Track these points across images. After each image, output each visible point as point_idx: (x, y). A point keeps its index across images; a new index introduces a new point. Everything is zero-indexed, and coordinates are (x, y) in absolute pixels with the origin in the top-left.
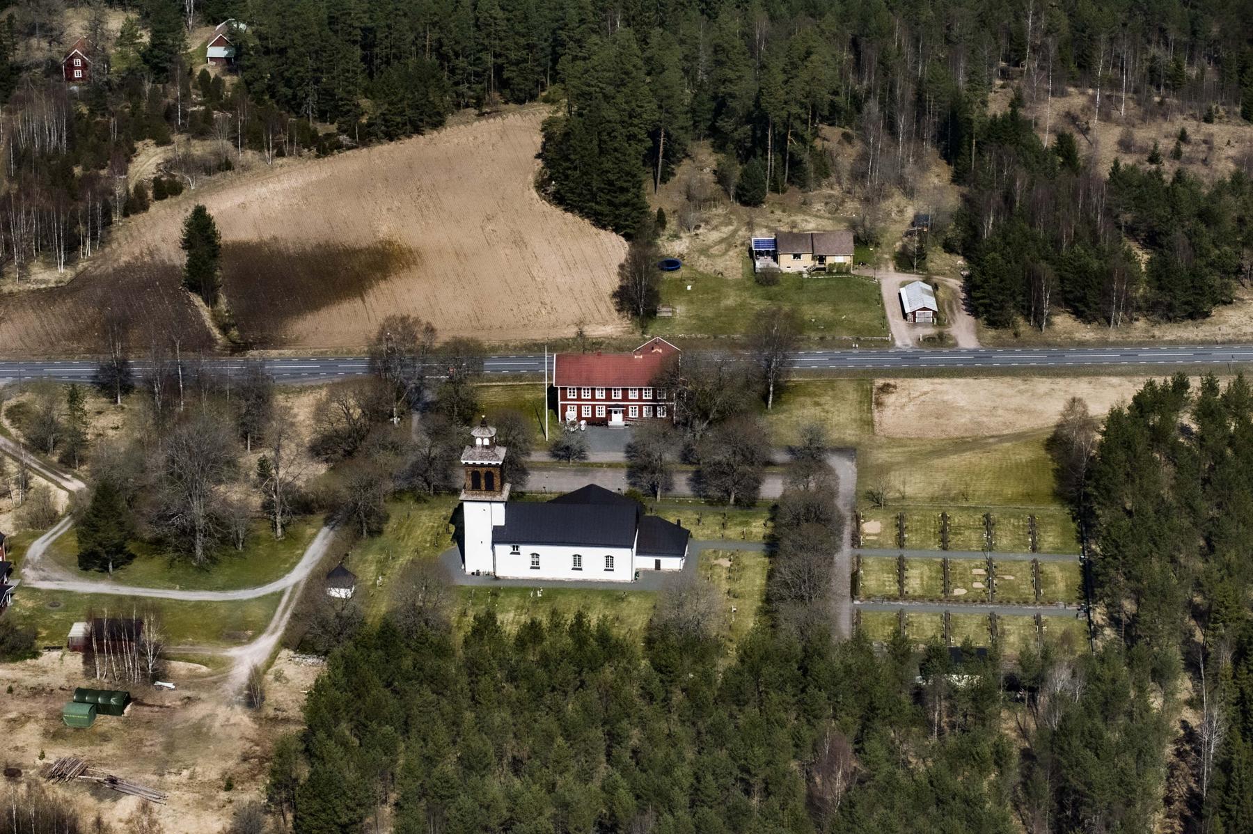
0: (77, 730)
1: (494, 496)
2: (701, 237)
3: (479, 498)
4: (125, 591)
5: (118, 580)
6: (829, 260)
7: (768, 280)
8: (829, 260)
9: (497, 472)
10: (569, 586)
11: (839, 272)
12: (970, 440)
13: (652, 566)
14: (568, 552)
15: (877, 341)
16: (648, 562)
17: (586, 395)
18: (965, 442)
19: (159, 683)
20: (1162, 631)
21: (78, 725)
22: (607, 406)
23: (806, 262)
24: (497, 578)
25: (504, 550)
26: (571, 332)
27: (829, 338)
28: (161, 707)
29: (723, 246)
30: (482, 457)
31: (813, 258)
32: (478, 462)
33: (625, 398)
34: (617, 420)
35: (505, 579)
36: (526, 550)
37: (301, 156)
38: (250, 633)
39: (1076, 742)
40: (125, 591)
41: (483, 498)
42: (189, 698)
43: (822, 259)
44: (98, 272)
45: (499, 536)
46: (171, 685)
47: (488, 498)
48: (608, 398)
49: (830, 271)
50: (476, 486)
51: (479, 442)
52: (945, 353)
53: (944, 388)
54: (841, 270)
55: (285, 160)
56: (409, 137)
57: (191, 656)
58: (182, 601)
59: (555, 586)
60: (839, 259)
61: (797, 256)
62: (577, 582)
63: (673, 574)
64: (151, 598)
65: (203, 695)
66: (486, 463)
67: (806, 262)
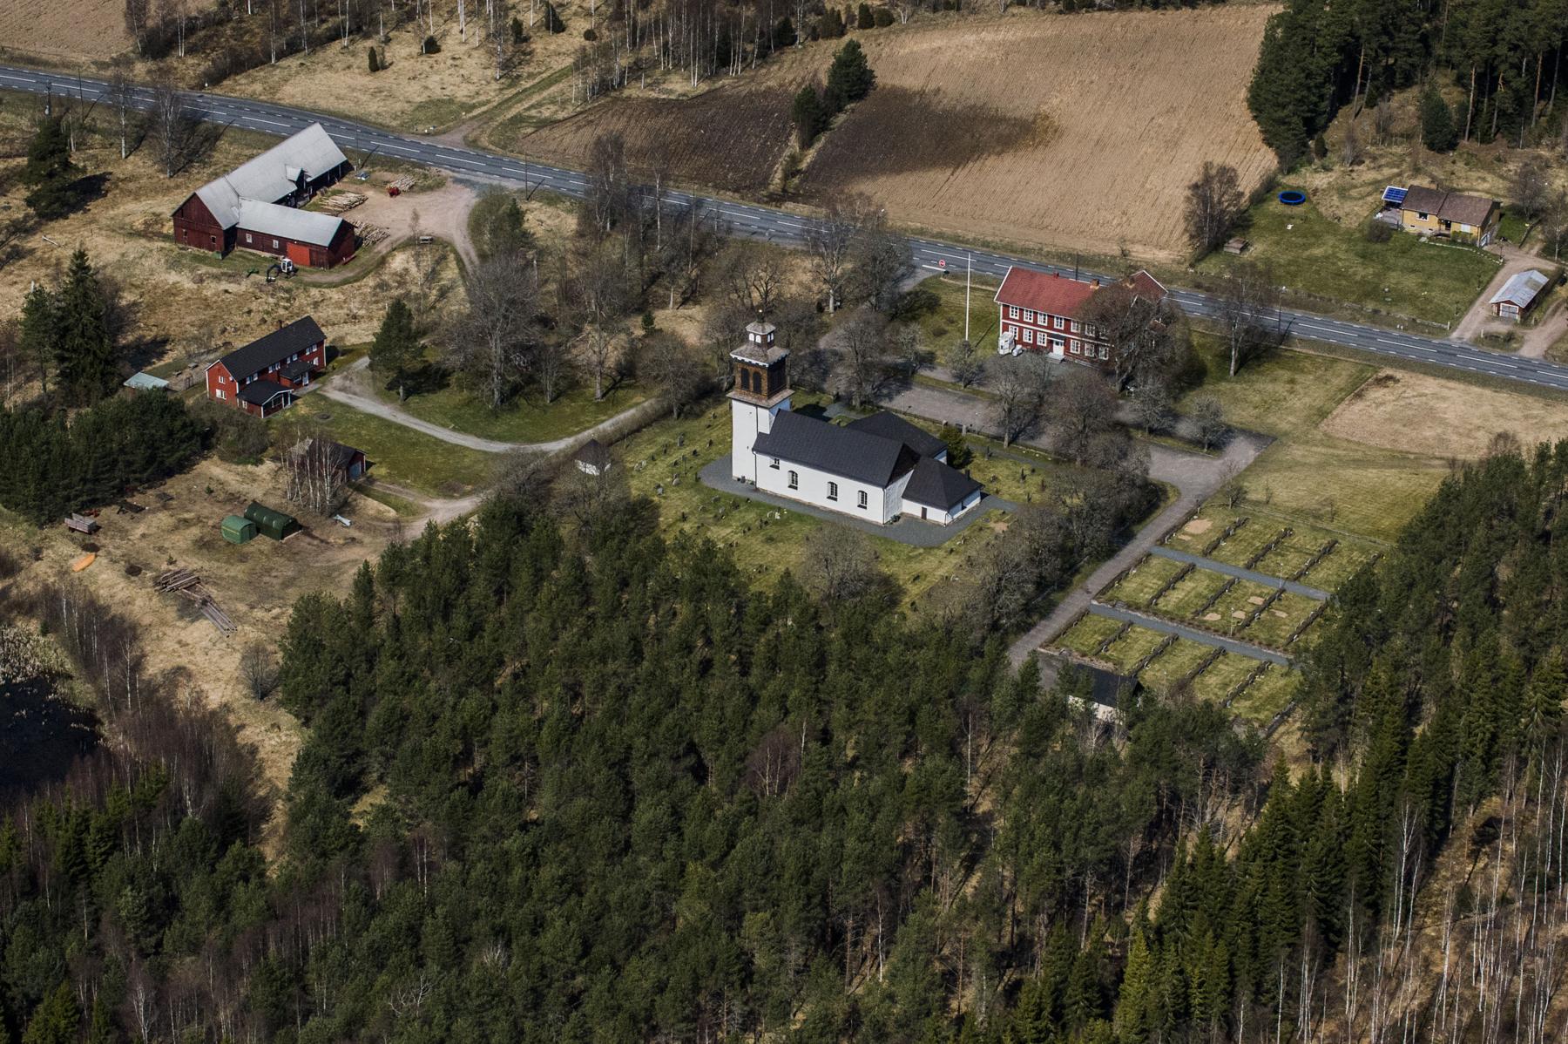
0: (229, 544)
1: (760, 399)
2: (1354, 175)
3: (745, 399)
4: (402, 419)
5: (405, 408)
6: (1455, 227)
7: (1381, 234)
8: (1455, 227)
9: (765, 375)
10: (815, 515)
11: (1463, 244)
12: (1412, 457)
13: (919, 514)
14: (825, 478)
15: (1434, 327)
16: (912, 508)
17: (1027, 317)
18: (1404, 458)
19: (339, 517)
20: (816, 789)
21: (231, 540)
22: (1049, 335)
23: (1430, 225)
24: (757, 490)
25: (766, 461)
26: (1115, 250)
27: (1384, 313)
28: (322, 541)
29: (1370, 189)
30: (751, 356)
31: (1440, 222)
32: (747, 360)
33: (1067, 330)
34: (1058, 351)
35: (764, 493)
36: (785, 466)
37: (1043, 8)
38: (469, 488)
39: (497, 922)
40: (402, 419)
41: (749, 399)
42: (353, 539)
43: (1448, 226)
44: (735, 91)
45: (763, 445)
46: (347, 522)
47: (754, 401)
48: (1050, 327)
49: (1454, 239)
50: (745, 385)
51: (751, 337)
52: (1494, 357)
53: (1446, 392)
54: (1465, 240)
55: (1022, 9)
56: (1178, 8)
57: (392, 500)
58: (442, 441)
59: (800, 510)
60: (1466, 228)
61: (1423, 215)
62: (832, 512)
63: (937, 525)
64: (416, 432)
65: (367, 540)
66: (754, 362)
67: (1430, 225)
